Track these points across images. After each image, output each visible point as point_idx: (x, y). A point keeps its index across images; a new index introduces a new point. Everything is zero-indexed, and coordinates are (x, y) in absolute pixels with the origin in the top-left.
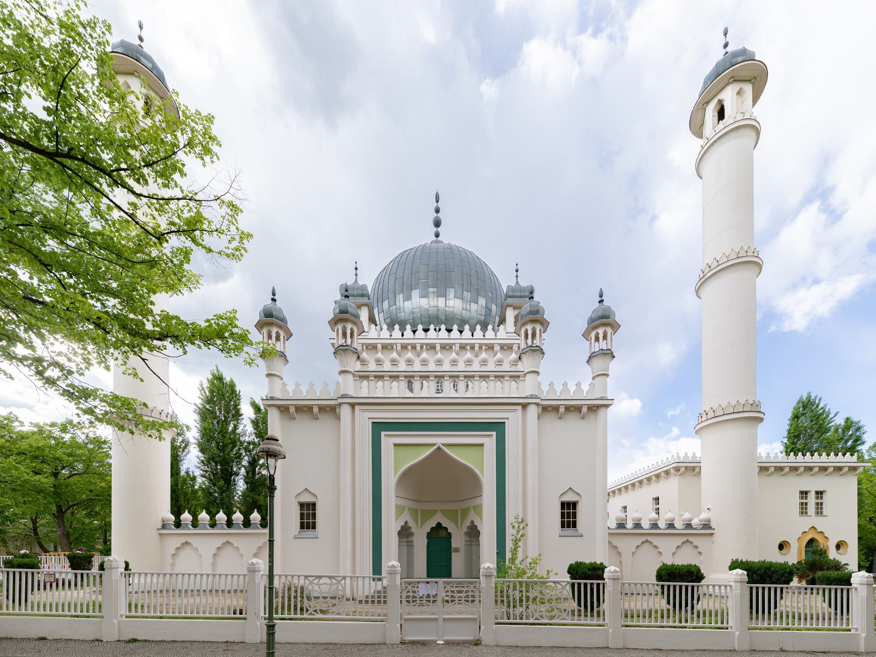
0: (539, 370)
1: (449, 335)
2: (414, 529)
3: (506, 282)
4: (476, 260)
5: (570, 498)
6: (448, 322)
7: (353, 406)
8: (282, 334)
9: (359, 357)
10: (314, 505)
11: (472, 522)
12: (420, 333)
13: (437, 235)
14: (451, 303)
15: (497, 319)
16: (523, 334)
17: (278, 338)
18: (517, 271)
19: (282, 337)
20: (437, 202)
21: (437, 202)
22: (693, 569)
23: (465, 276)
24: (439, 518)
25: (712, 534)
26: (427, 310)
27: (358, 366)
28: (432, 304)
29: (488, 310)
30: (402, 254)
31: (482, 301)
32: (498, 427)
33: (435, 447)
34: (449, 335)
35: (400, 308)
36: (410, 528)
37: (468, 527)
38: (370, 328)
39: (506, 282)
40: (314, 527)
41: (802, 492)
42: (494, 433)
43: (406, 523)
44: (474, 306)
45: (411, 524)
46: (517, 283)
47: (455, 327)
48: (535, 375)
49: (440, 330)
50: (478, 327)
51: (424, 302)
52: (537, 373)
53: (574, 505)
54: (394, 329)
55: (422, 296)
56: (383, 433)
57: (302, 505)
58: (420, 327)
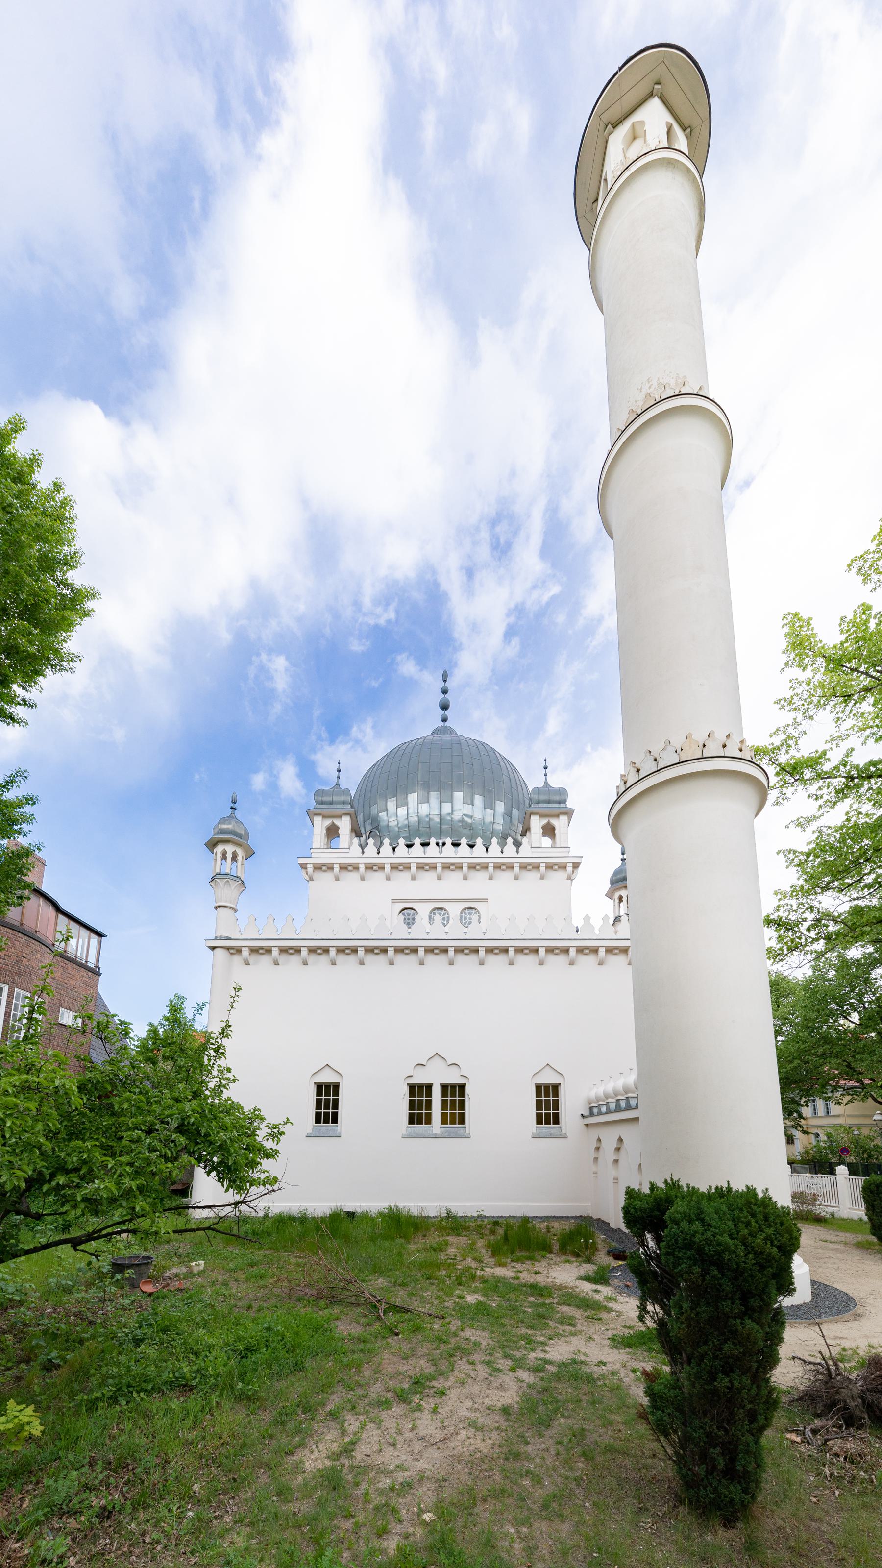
0: (237, 908)
1: (456, 852)
3: (534, 782)
4: (491, 754)
8: (240, 853)
10: (336, 1086)
12: (402, 849)
13: (444, 720)
15: (520, 827)
17: (234, 858)
18: (546, 768)
19: (239, 858)
20: (445, 681)
21: (445, 681)
25: (636, 1119)
30: (399, 747)
31: (500, 807)
34: (456, 852)
38: (351, 844)
39: (534, 782)
40: (335, 1120)
41: (455, 1094)
46: (546, 783)
47: (464, 841)
48: (231, 912)
49: (444, 844)
50: (494, 840)
51: (424, 809)
52: (236, 911)
54: (506, 844)
55: (421, 801)
57: (319, 1087)
58: (402, 842)
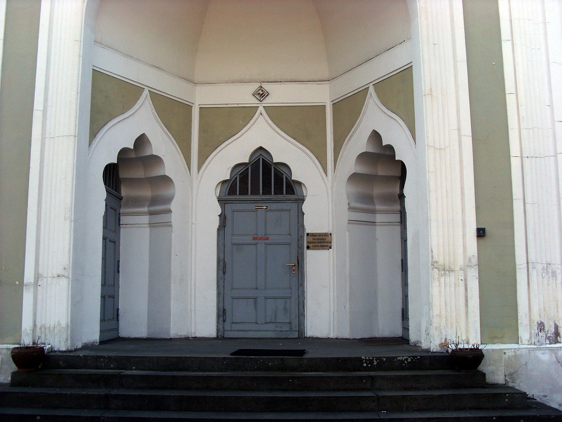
11: (376, 136)
24: (261, 135)
36: (156, 160)
37: (364, 157)
43: (141, 141)
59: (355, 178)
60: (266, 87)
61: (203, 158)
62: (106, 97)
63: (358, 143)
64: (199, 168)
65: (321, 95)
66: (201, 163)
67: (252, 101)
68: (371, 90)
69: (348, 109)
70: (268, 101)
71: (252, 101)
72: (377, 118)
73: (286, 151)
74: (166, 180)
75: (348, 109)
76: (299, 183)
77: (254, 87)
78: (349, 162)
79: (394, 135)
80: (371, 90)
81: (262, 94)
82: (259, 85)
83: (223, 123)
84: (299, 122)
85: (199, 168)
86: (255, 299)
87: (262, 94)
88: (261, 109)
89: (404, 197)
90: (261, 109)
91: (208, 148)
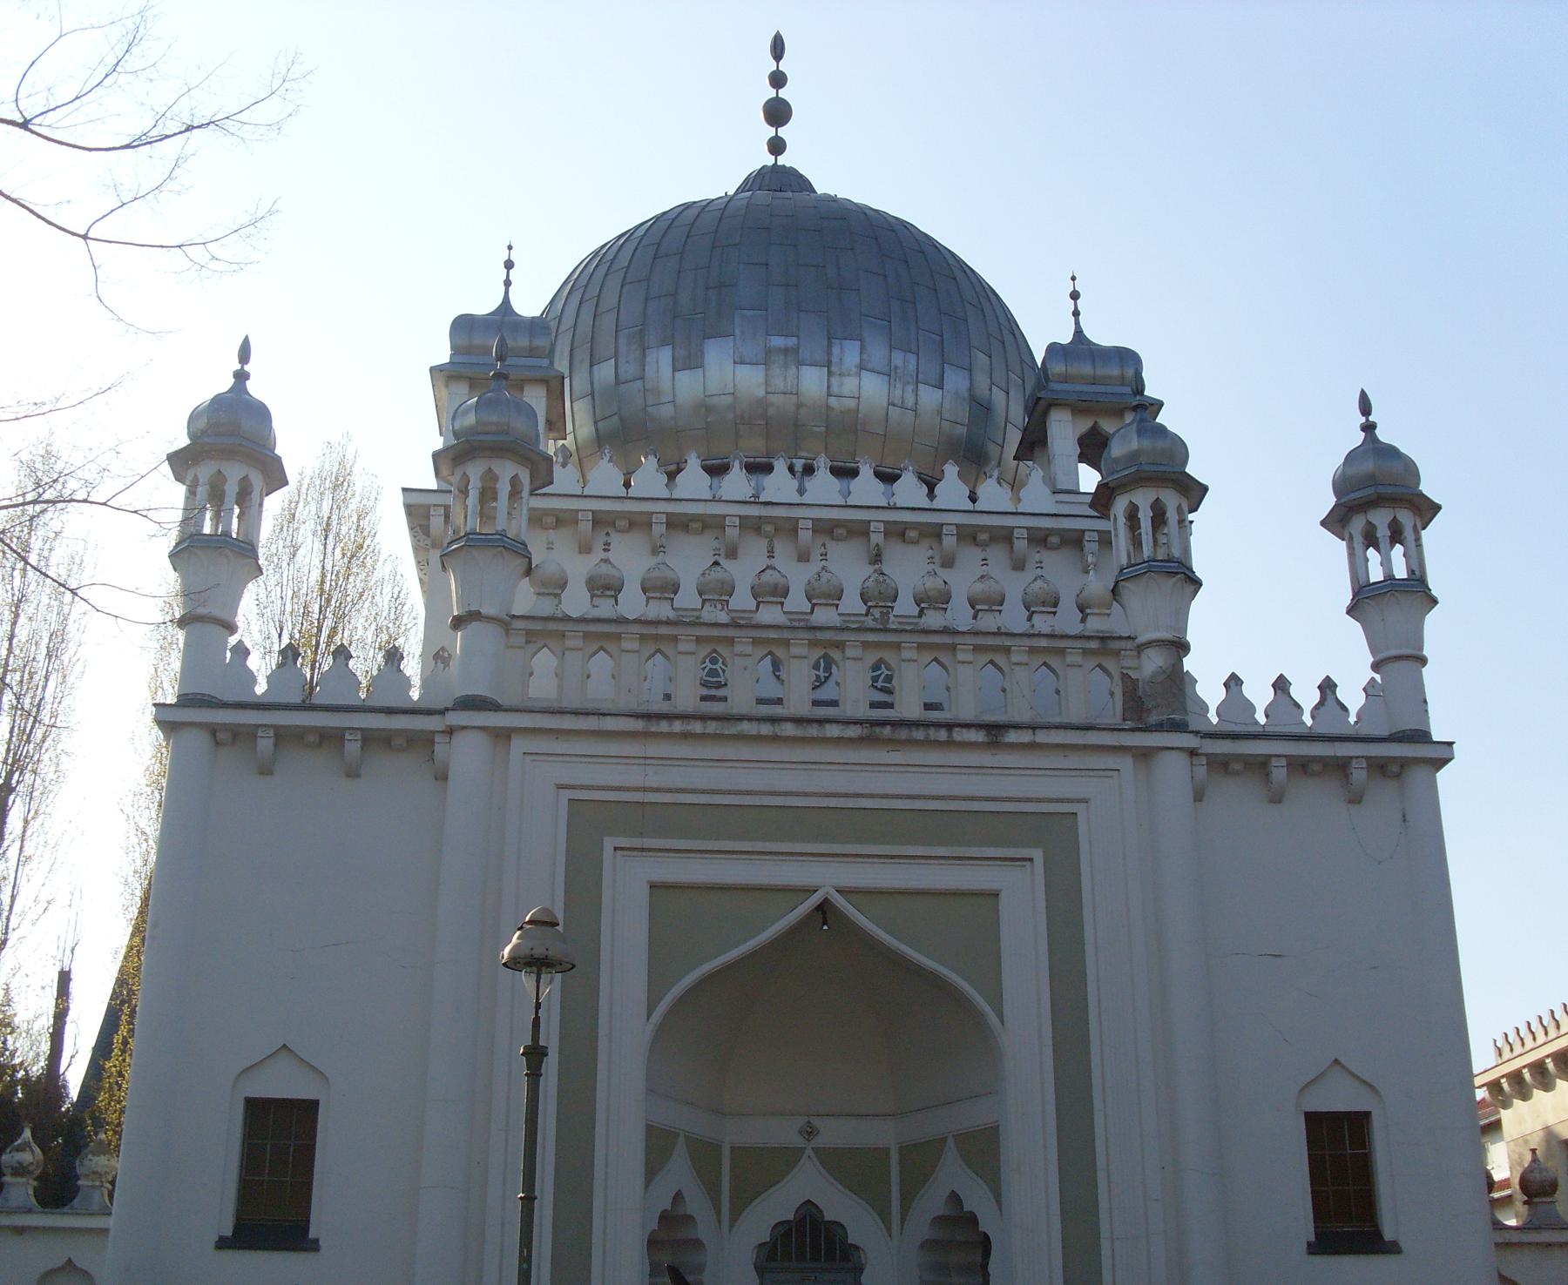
2: (704, 1229)
3: (1043, 330)
5: (1338, 1098)
6: (841, 443)
7: (502, 736)
9: (529, 571)
11: (955, 1198)
14: (849, 385)
16: (1122, 520)
22: (202, 423)
23: (914, 349)
24: (807, 1185)
26: (762, 403)
27: (525, 599)
28: (779, 383)
29: (981, 409)
32: (1051, 833)
33: (815, 900)
35: (657, 392)
36: (689, 1219)
37: (939, 1221)
39: (1043, 330)
42: (1037, 854)
43: (678, 1197)
44: (929, 398)
45: (696, 1204)
53: (1358, 1123)
56: (609, 843)
59: (927, 1245)
60: (816, 1122)
61: (736, 1214)
62: (658, 1145)
63: (932, 1203)
64: (731, 1226)
65: (884, 1135)
66: (733, 1220)
67: (799, 1141)
68: (951, 1142)
69: (920, 1160)
70: (822, 1141)
71: (799, 1141)
72: (953, 1175)
73: (839, 1205)
74: (697, 1244)
75: (920, 1160)
76: (857, 1248)
77: (800, 1122)
78: (921, 1224)
79: (977, 1200)
80: (951, 1142)
81: (809, 1132)
82: (806, 1119)
83: (759, 1170)
84: (857, 1169)
85: (731, 1226)
86: (1336, 1061)
87: (809, 1132)
88: (809, 1152)
89: (1342, 485)
90: (809, 1152)
91: (744, 1196)
